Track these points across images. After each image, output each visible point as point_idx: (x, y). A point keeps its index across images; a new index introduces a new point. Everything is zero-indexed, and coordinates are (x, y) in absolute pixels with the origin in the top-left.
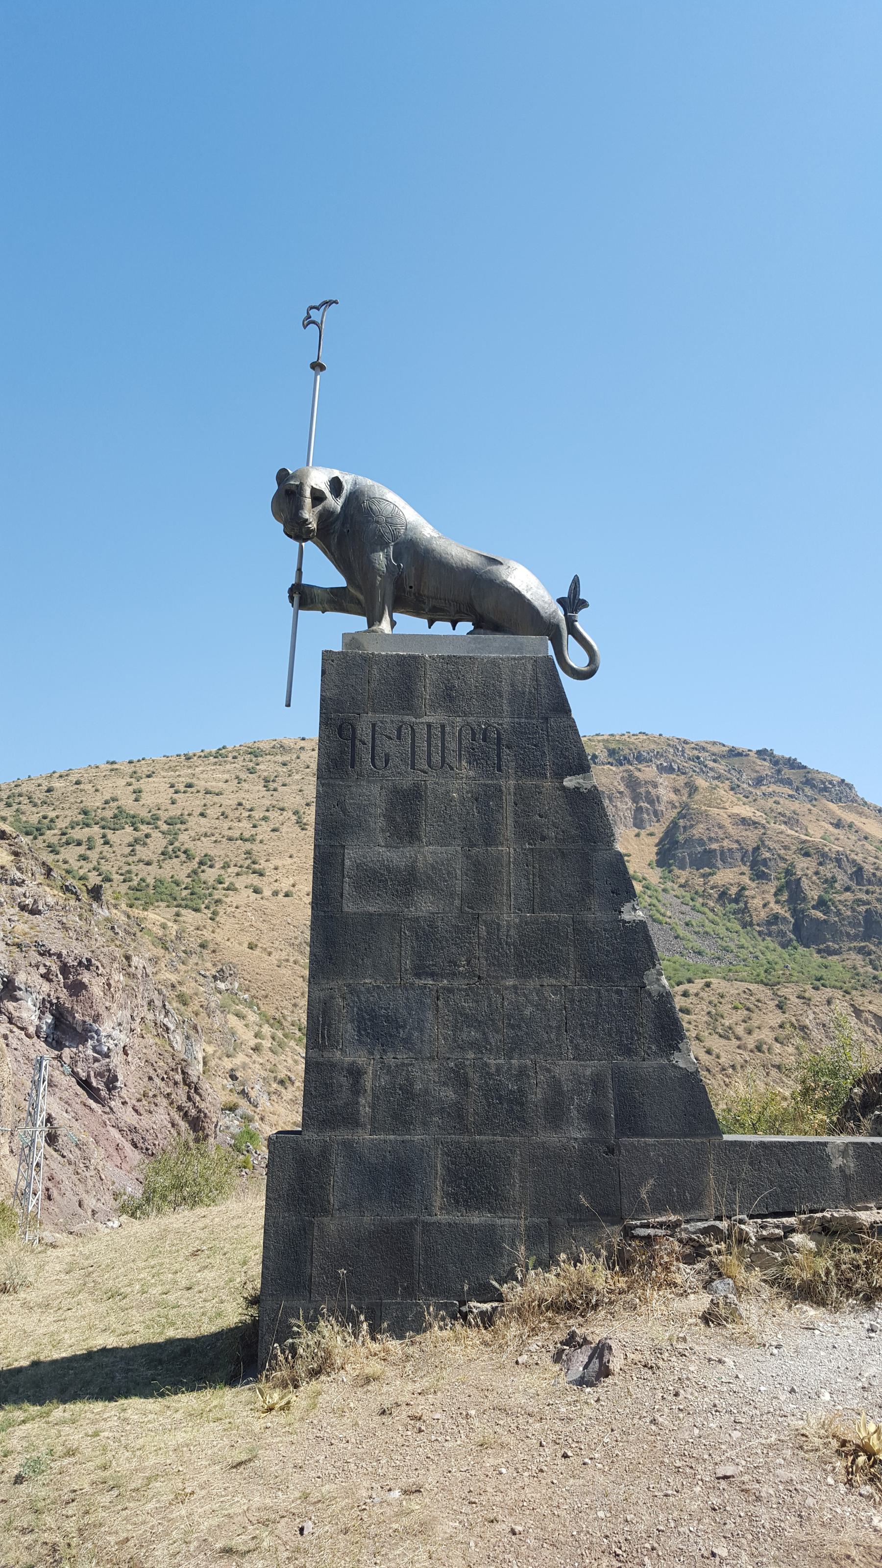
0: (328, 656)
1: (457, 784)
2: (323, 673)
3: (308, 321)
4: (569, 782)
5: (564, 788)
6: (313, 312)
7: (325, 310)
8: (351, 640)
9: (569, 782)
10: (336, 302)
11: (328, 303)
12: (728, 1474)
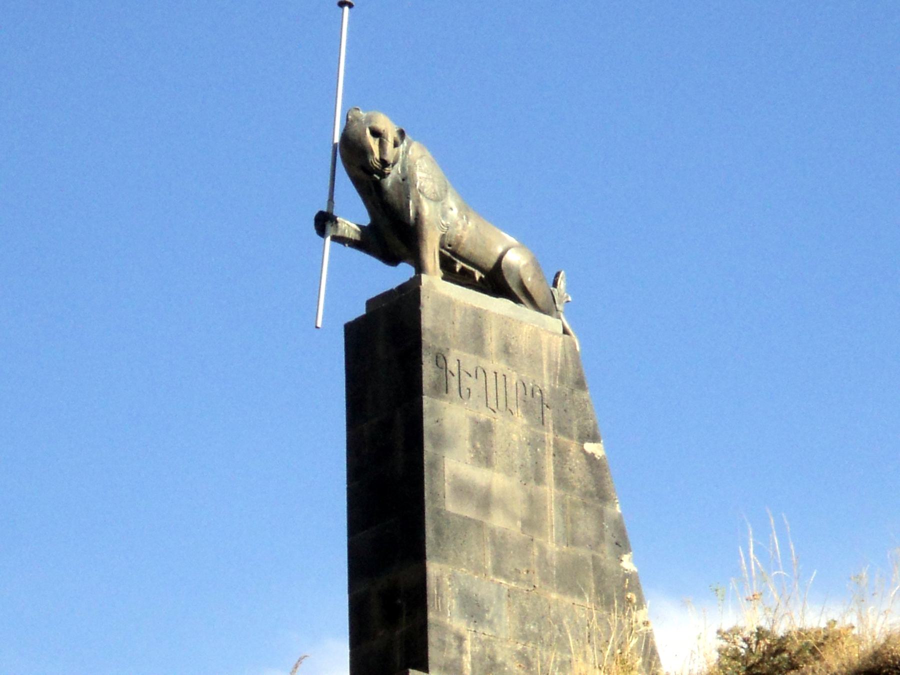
1: (516, 427)
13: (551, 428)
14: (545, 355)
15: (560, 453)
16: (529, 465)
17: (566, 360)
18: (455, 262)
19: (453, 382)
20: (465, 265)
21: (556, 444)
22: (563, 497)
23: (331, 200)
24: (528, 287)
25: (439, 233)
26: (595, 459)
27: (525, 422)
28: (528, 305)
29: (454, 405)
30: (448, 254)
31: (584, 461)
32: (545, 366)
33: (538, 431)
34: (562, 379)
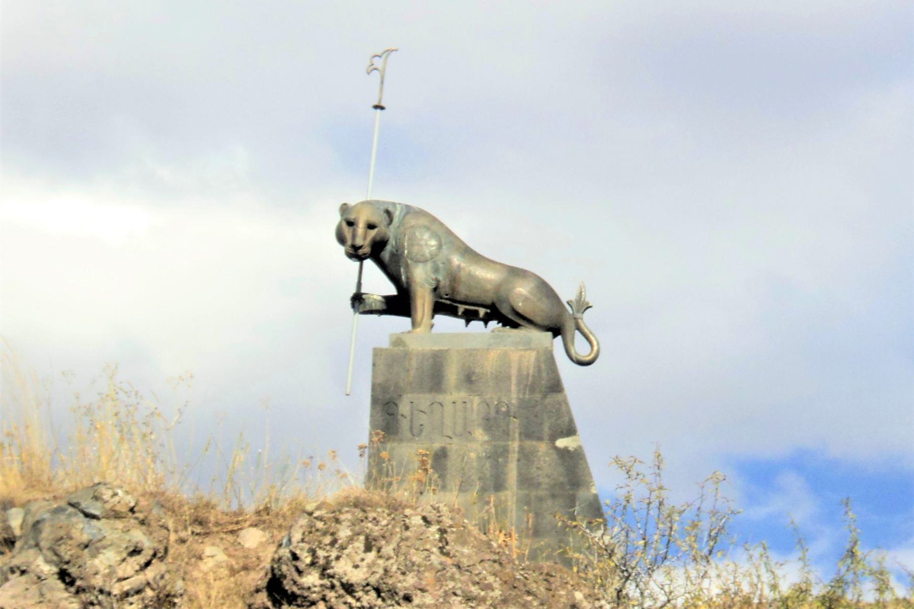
0: (377, 352)
1: (475, 446)
2: (374, 365)
3: (372, 69)
4: (561, 443)
5: (556, 448)
6: (376, 60)
7: (386, 58)
8: (398, 341)
9: (561, 443)
10: (617, 460)
11: (389, 51)
12: (149, 568)
13: (517, 435)
14: (514, 372)
15: (526, 457)
16: (488, 476)
17: (539, 371)
18: (457, 307)
19: (405, 424)
20: (467, 307)
21: (522, 449)
22: (528, 496)
23: (359, 284)
24: (521, 311)
25: (428, 288)
26: (569, 451)
27: (486, 438)
28: (527, 325)
29: (404, 445)
30: (448, 302)
31: (555, 456)
32: (514, 380)
33: (502, 443)
34: (532, 389)
